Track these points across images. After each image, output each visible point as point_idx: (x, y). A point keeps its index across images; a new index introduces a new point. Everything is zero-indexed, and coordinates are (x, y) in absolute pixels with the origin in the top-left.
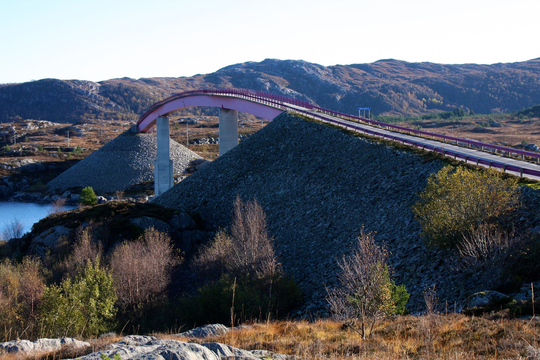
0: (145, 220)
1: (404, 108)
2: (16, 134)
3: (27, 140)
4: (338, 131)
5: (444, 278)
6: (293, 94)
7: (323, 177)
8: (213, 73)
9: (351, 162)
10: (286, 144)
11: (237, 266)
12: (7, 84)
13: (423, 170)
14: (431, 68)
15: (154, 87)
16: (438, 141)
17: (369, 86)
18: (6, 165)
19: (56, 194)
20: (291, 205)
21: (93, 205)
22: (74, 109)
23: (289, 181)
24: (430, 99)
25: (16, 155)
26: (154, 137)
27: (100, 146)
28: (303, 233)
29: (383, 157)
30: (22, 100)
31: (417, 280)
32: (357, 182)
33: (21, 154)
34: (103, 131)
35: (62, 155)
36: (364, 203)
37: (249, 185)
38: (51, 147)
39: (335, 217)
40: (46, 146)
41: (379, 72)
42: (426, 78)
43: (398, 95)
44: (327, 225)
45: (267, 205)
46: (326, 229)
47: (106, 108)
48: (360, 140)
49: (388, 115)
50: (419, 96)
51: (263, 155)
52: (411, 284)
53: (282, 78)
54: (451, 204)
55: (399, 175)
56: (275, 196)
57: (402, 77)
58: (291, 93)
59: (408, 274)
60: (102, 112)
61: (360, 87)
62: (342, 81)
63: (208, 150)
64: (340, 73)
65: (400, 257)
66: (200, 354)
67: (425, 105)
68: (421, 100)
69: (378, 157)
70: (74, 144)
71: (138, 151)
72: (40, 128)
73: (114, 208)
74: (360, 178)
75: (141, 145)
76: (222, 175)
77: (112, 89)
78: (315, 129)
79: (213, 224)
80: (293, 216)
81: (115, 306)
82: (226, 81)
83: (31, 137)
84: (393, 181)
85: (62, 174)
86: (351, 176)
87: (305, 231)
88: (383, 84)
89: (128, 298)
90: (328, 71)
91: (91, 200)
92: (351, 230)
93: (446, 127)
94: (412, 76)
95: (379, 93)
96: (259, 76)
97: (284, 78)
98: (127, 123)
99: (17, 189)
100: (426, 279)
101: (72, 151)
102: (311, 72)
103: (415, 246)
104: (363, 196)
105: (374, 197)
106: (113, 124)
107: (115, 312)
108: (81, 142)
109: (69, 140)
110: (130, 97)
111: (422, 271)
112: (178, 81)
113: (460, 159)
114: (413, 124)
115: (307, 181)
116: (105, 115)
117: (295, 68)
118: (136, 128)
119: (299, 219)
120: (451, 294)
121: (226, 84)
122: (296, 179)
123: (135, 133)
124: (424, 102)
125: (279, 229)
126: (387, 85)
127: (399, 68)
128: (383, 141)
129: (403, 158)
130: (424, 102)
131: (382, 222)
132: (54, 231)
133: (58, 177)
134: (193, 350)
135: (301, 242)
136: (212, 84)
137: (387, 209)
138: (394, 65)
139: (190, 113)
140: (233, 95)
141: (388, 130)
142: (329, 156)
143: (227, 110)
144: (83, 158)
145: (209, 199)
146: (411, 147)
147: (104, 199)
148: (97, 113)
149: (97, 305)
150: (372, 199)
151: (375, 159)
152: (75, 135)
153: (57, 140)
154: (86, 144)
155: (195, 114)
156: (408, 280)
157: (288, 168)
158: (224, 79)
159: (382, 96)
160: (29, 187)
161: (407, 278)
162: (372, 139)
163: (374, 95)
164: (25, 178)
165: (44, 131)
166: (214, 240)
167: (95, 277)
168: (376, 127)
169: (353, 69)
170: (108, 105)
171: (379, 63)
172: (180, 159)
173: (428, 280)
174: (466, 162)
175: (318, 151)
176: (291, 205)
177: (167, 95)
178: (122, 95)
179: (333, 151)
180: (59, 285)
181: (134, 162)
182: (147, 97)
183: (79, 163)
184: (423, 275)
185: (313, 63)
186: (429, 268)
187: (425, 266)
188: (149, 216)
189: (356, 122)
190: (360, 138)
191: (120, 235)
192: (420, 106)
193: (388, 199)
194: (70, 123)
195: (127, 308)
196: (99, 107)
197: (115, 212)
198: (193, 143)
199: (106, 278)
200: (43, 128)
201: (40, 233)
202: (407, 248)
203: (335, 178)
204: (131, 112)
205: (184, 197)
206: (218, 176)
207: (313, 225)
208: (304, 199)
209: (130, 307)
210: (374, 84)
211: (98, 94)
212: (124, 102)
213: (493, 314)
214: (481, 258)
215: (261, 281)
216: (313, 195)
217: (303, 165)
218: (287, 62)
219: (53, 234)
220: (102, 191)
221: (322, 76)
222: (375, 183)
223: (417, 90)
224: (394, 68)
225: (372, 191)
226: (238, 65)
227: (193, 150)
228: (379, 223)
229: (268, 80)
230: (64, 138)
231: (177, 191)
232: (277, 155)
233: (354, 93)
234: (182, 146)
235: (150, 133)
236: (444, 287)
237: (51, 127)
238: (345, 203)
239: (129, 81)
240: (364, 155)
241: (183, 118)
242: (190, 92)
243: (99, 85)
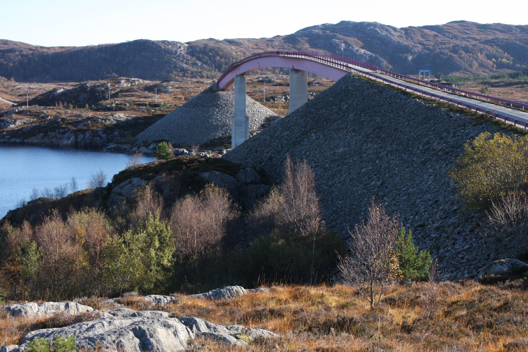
0: (213, 174)
1: (474, 67)
2: (111, 90)
3: (120, 96)
4: (398, 93)
5: (477, 241)
6: (366, 54)
7: (380, 137)
8: (292, 35)
9: (407, 123)
10: (349, 104)
11: (286, 222)
12: (106, 44)
13: (473, 133)
14: (502, 29)
15: (236, 47)
16: (493, 103)
17: (440, 46)
18: (100, 118)
19: (143, 146)
20: (349, 163)
21: (168, 159)
22: (164, 67)
23: (349, 140)
24: (500, 59)
25: (110, 109)
26: (232, 95)
27: (185, 102)
28: (357, 190)
29: (437, 119)
30: (118, 59)
31: (452, 242)
32: (411, 143)
33: (114, 109)
34: (188, 88)
35: (150, 110)
36: (415, 163)
37: (312, 143)
38: (141, 103)
39: (387, 176)
40: (136, 102)
41: (450, 33)
42: (497, 39)
43: (468, 56)
44: (379, 183)
45: (327, 162)
46: (378, 187)
47: (193, 67)
48: (417, 102)
49: (457, 74)
50: (489, 57)
51: (326, 114)
52: (447, 246)
53: (356, 39)
54: (487, 169)
55: (450, 136)
56: (334, 154)
57: (473, 38)
58: (364, 53)
59: (445, 235)
60: (189, 70)
61: (431, 48)
62: (414, 42)
63: (283, 107)
64: (412, 34)
65: (440, 218)
66: (171, 331)
67: (495, 65)
68: (491, 60)
69: (432, 118)
70: (161, 100)
71: (218, 108)
72: (132, 85)
73: (185, 162)
74: (414, 138)
75: (221, 102)
76: (288, 132)
77: (198, 49)
78: (376, 91)
79: (277, 179)
80: (349, 173)
81: (173, 256)
82: (303, 42)
83: (124, 94)
84: (445, 142)
85: (149, 128)
86: (406, 137)
87: (359, 188)
88: (454, 44)
89: (186, 248)
90: (401, 32)
91: (165, 155)
92: (400, 189)
93: (515, 86)
94: (483, 36)
95: (450, 53)
96: (335, 37)
97: (358, 39)
98: (210, 81)
99: (110, 141)
100: (461, 241)
101: (159, 107)
102: (384, 33)
103: (455, 208)
104: (415, 156)
105: (425, 157)
106: (197, 82)
107: (173, 261)
108: (168, 99)
109: (157, 96)
110: (214, 57)
111: (459, 233)
112: (259, 41)
113: (510, 123)
114: (482, 83)
115: (365, 141)
116: (192, 73)
117: (369, 30)
118: (216, 86)
119: (354, 177)
120: (481, 257)
121: (303, 44)
122: (355, 138)
123: (215, 91)
124: (494, 62)
125: (335, 185)
126: (458, 46)
127: (470, 29)
128: (439, 103)
129: (456, 121)
130: (494, 62)
131: (429, 183)
132: (131, 182)
133: (146, 130)
134: (165, 326)
135: (355, 198)
136: (290, 45)
137: (436, 169)
138: (465, 26)
139: (268, 72)
140: (303, 57)
141: (446, 92)
142: (388, 116)
143: (297, 71)
144: (169, 113)
145: (274, 155)
146: (465, 109)
147: (185, 151)
148: (184, 71)
149: (156, 254)
150: (423, 159)
151: (429, 120)
152: (162, 92)
153: (147, 96)
154: (172, 100)
155: (274, 73)
156: (445, 241)
157: (349, 127)
158: (302, 40)
159: (452, 57)
160: (120, 139)
161: (444, 239)
162: (429, 100)
163: (444, 55)
164: (117, 131)
165: (135, 88)
166: (268, 196)
167: (155, 228)
168: (434, 89)
169: (425, 30)
170: (194, 64)
171: (451, 24)
172: (256, 115)
173: (463, 242)
174: (515, 125)
175: (378, 111)
176: (349, 163)
177: (248, 54)
178: (207, 55)
179: (392, 112)
180: (121, 236)
181: (213, 118)
182: (230, 57)
183: (164, 118)
184: (459, 237)
185: (387, 25)
186: (465, 230)
187: (463, 227)
188: (217, 171)
189: (416, 84)
190: (418, 100)
191: (190, 187)
192: (490, 67)
193: (438, 161)
194: (159, 81)
195: (183, 259)
196: (186, 65)
197: (186, 166)
198: (269, 101)
199: (165, 230)
200: (135, 85)
201: (120, 183)
202: (448, 209)
203: (390, 138)
204: (216, 71)
205: (252, 153)
206: (284, 133)
207: (367, 182)
208: (361, 158)
209: (187, 257)
210: (445, 45)
211: (186, 53)
212: (209, 61)
213: (508, 283)
214: (511, 225)
215: (305, 238)
216: (370, 154)
217: (362, 125)
218: (362, 24)
219: (131, 185)
220: (184, 144)
221: (395, 38)
222: (428, 144)
223: (488, 50)
224: (465, 29)
225: (424, 151)
226: (315, 27)
227: (269, 107)
228: (427, 184)
229: (342, 41)
230: (153, 95)
231: (246, 147)
232: (340, 114)
233: (425, 53)
234: (258, 103)
235: (229, 91)
236: (476, 250)
237: (141, 84)
238: (397, 162)
239: (214, 42)
240: (420, 116)
241: (262, 77)
242: (268, 53)
243: (187, 45)
